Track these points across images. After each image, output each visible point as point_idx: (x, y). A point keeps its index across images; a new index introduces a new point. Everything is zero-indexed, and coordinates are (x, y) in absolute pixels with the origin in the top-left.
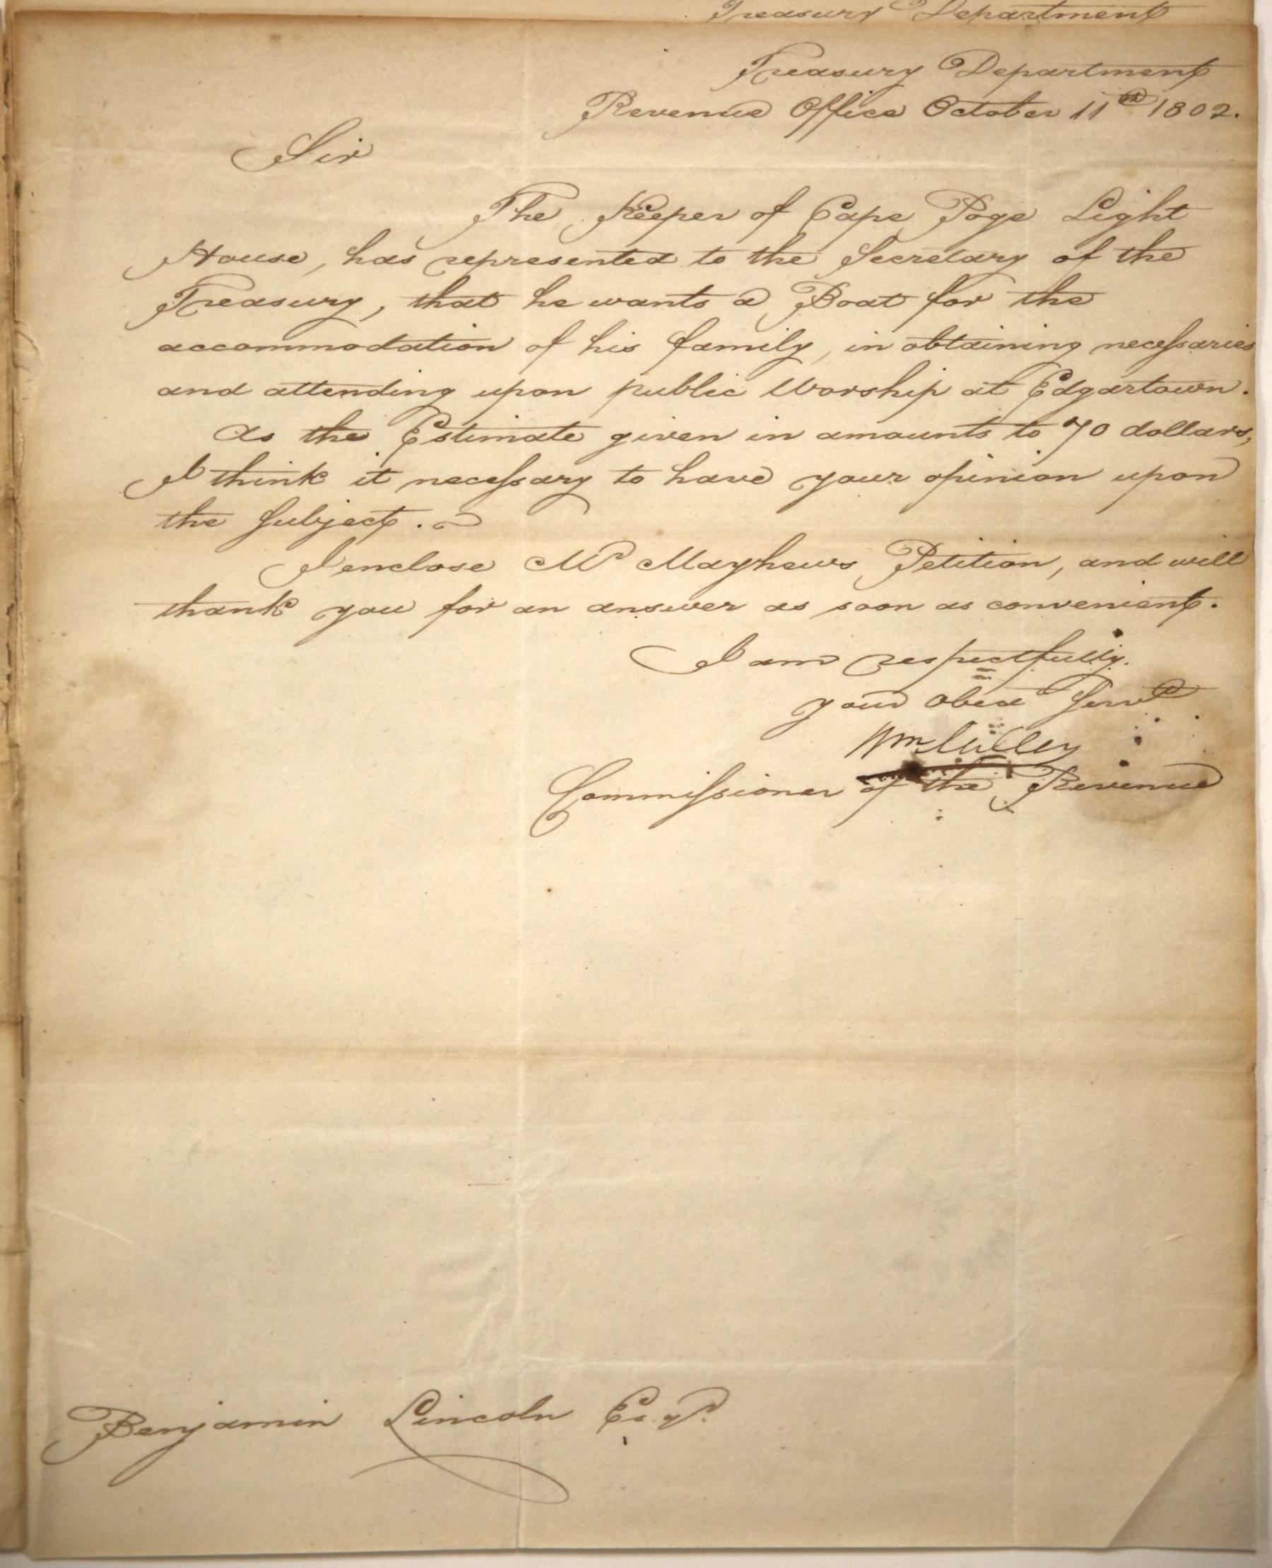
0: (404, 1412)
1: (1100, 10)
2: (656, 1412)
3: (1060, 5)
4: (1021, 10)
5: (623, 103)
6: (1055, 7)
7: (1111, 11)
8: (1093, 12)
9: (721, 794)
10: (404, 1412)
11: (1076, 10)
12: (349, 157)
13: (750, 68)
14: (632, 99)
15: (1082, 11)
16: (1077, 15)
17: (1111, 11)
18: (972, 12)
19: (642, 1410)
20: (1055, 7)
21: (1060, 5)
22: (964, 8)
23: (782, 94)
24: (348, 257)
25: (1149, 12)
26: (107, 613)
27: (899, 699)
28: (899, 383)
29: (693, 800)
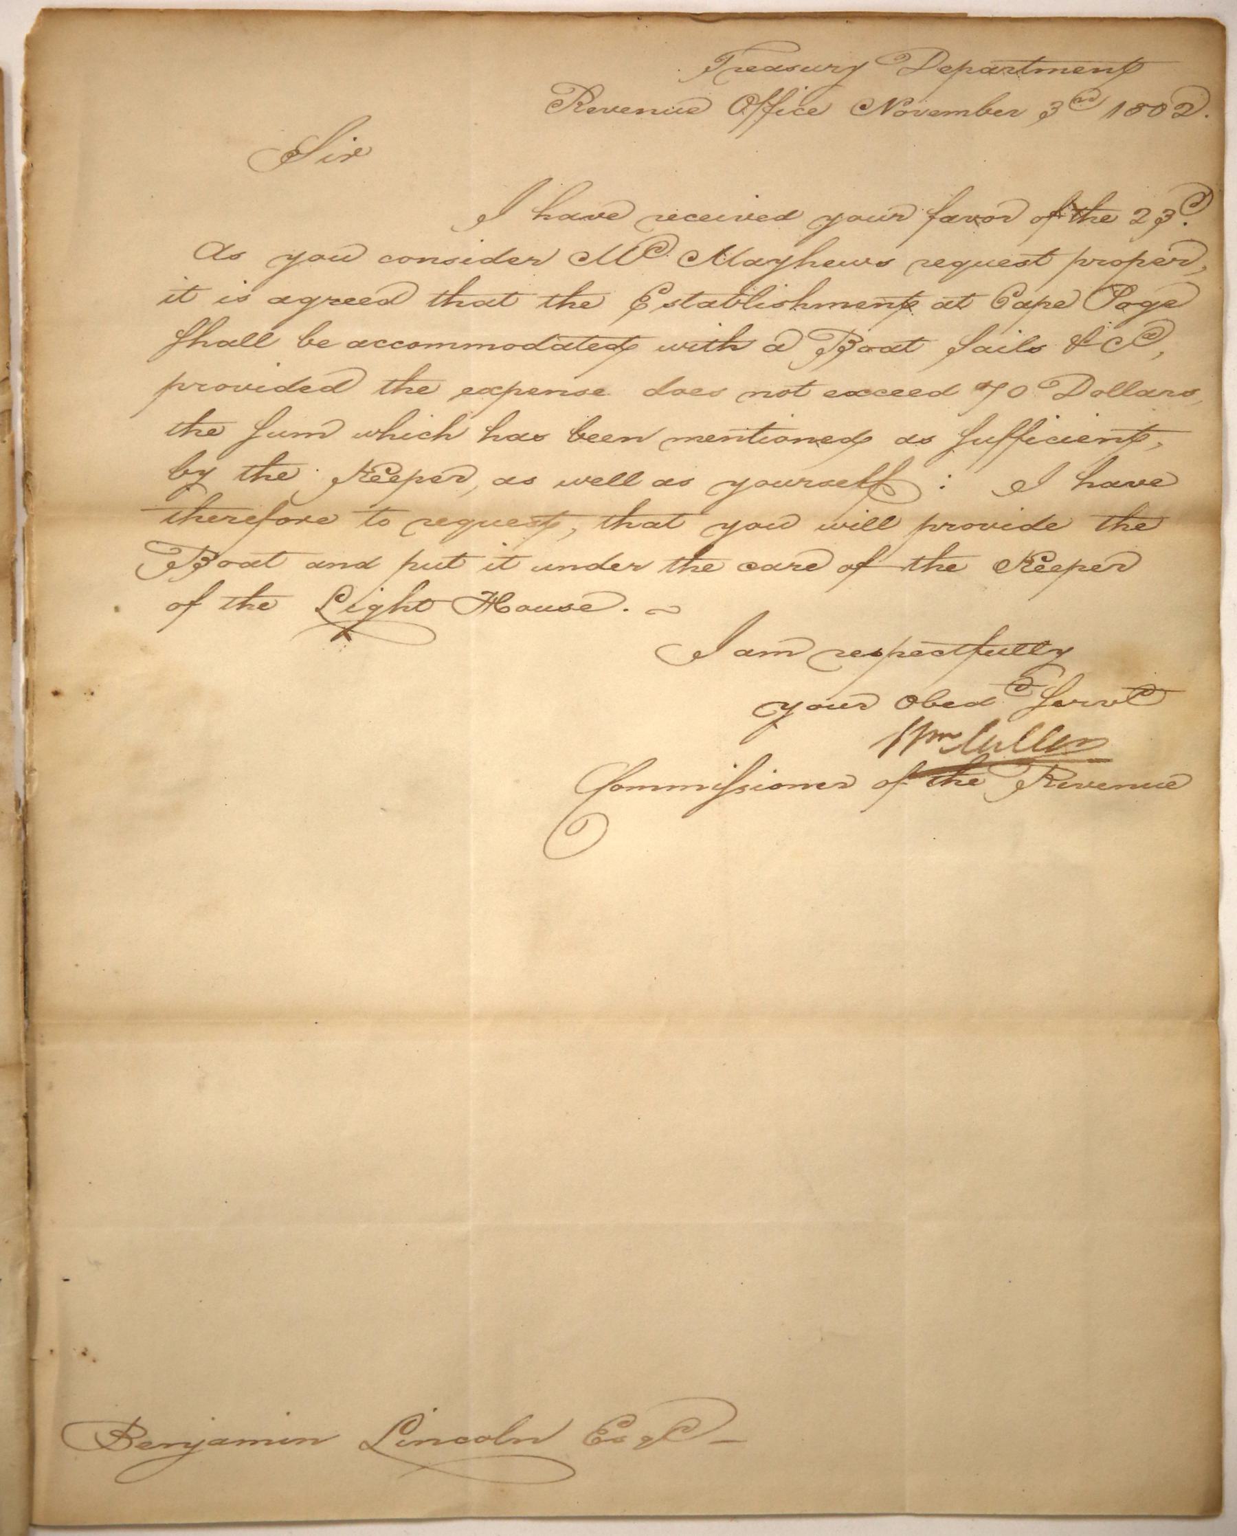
0: (392, 1431)
1: (1077, 65)
2: (634, 1434)
3: (1039, 60)
4: (1001, 65)
5: (587, 101)
6: (1034, 62)
7: (1088, 67)
8: (1071, 67)
9: (743, 789)
10: (392, 1431)
11: (1054, 66)
12: (350, 156)
13: (713, 65)
14: (593, 98)
15: (1060, 66)
16: (1055, 70)
17: (1088, 67)
18: (954, 67)
19: (620, 1432)
20: (1034, 62)
21: (1039, 60)
22: (947, 63)
23: (735, 86)
24: (1078, 482)
25: (1125, 67)
26: (113, 611)
27: (1095, 94)
28: (450, 427)
29: (721, 791)
